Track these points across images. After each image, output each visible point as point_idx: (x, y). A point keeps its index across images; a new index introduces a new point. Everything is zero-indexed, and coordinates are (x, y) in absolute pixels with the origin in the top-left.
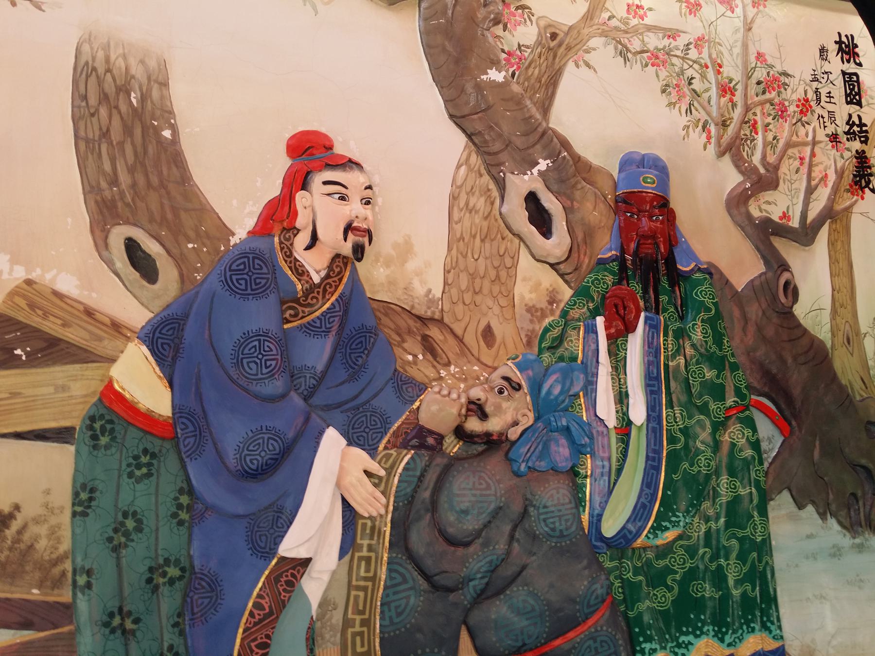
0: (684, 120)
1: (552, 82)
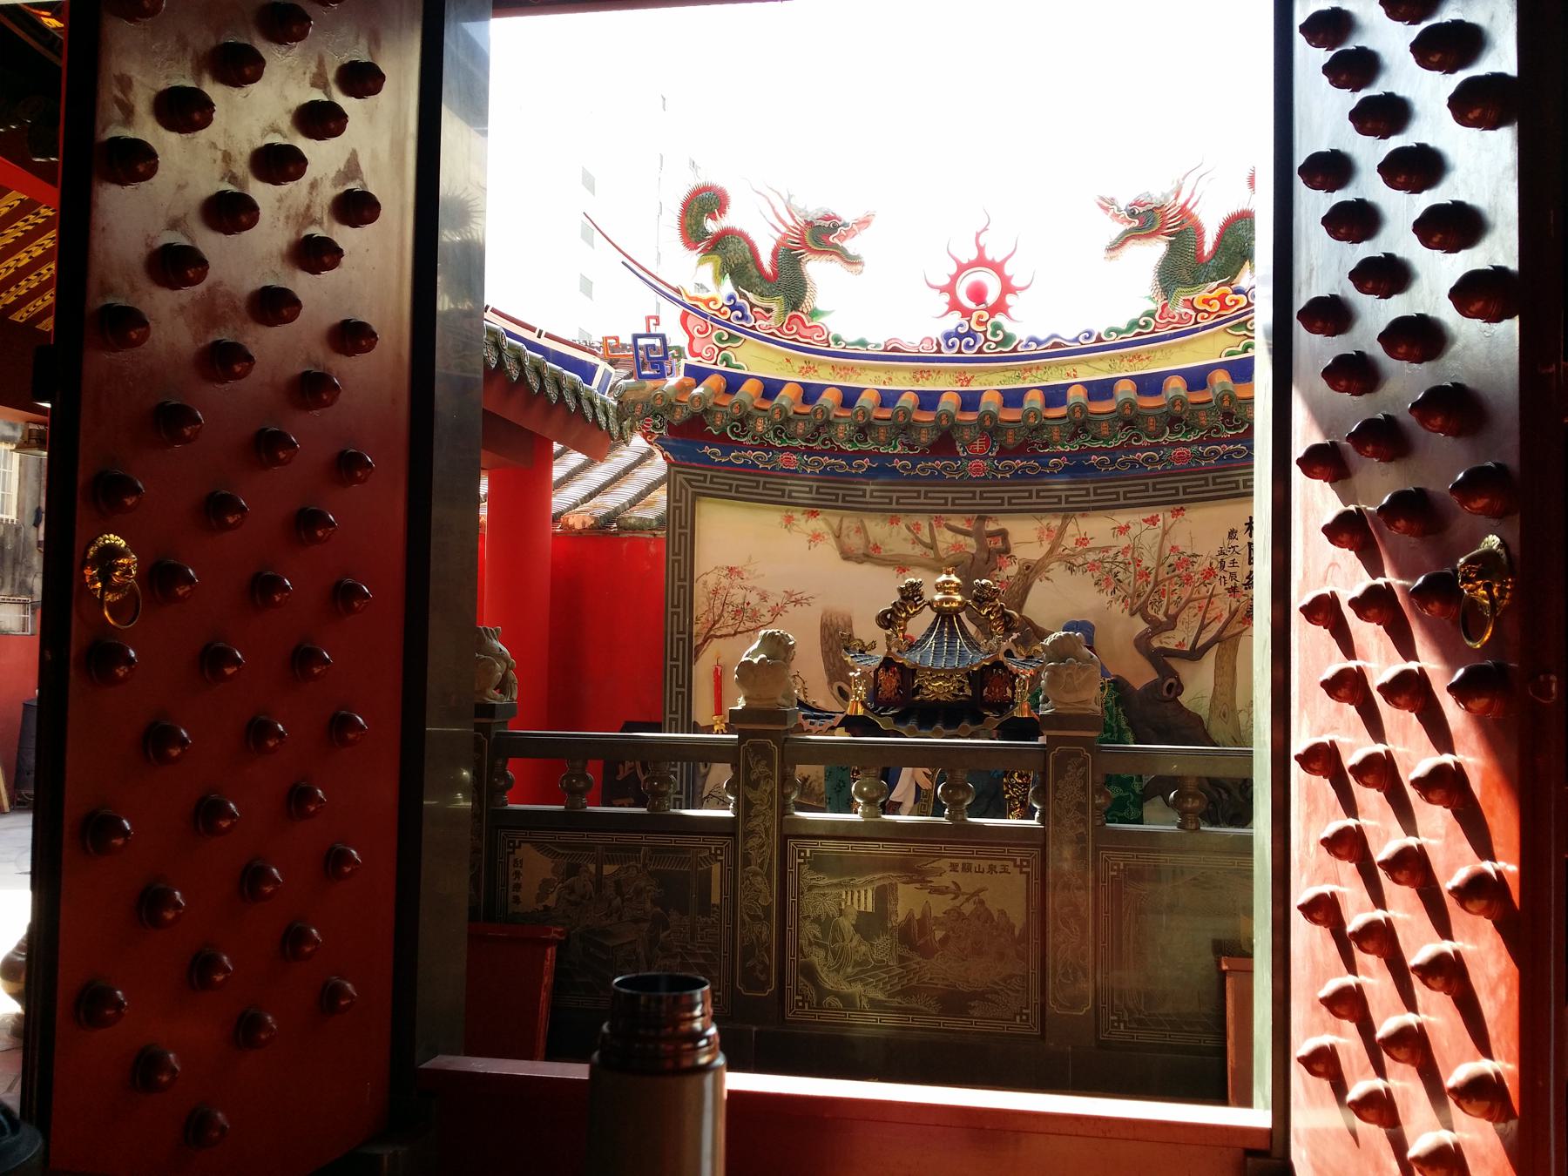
0: (1110, 598)
1: (1026, 590)
